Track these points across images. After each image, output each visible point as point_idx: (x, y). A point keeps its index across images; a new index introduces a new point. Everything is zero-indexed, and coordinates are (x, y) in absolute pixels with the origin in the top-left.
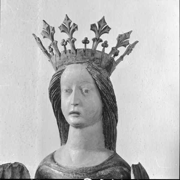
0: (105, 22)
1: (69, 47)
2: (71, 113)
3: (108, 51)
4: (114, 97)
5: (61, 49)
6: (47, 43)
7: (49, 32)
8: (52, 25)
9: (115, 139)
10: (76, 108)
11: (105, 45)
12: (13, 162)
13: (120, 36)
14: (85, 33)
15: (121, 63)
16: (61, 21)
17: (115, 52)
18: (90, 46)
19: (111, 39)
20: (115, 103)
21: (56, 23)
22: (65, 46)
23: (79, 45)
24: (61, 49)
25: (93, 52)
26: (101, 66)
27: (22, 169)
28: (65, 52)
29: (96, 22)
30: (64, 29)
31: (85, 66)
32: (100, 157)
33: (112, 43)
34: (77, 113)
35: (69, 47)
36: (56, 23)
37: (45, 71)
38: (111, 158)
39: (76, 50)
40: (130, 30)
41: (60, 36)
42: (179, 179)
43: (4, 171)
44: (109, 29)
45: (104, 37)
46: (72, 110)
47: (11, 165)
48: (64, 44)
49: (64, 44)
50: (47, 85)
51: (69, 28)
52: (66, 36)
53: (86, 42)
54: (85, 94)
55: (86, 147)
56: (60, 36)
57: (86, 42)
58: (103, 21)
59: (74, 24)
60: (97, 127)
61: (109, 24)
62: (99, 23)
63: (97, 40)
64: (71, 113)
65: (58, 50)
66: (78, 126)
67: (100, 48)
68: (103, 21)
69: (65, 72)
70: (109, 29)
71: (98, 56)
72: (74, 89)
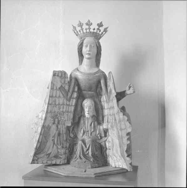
0: (102, 23)
2: (87, 54)
3: (100, 33)
4: (101, 49)
5: (85, 31)
6: (78, 29)
8: (82, 22)
10: (89, 52)
11: (100, 31)
12: (62, 70)
13: (105, 28)
14: (94, 26)
15: (103, 37)
16: (78, 23)
17: (102, 33)
18: (95, 31)
19: (102, 29)
21: (84, 21)
23: (92, 30)
24: (85, 31)
25: (96, 33)
26: (97, 36)
27: (65, 73)
28: (86, 32)
29: (91, 21)
30: (87, 24)
31: (93, 38)
32: (96, 70)
33: (102, 31)
34: (89, 54)
37: (77, 41)
38: (99, 70)
39: (90, 32)
41: (85, 27)
42: (185, 186)
43: (58, 73)
44: (103, 25)
45: (100, 28)
46: (88, 53)
47: (61, 71)
48: (86, 29)
49: (86, 29)
51: (89, 24)
52: (87, 27)
53: (94, 29)
55: (91, 66)
56: (85, 27)
57: (94, 29)
58: (101, 23)
59: (91, 23)
60: (94, 60)
61: (103, 24)
62: (100, 23)
63: (98, 29)
64: (87, 54)
65: (83, 32)
66: (89, 59)
67: (98, 32)
68: (101, 23)
69: (86, 39)
70: (103, 25)
71: (97, 35)
72: (89, 46)
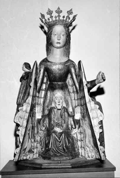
1: (57, 19)
7: (43, 16)
9: (35, 86)
14: (64, 14)
15: (73, 31)
19: (71, 17)
20: (101, 145)
21: (54, 9)
22: (56, 18)
23: (61, 18)
35: (57, 19)
36: (54, 9)
40: (40, 20)
48: (56, 17)
49: (56, 17)
50: (13, 122)
52: (57, 15)
53: (49, 19)
54: (61, 98)
57: (64, 17)
